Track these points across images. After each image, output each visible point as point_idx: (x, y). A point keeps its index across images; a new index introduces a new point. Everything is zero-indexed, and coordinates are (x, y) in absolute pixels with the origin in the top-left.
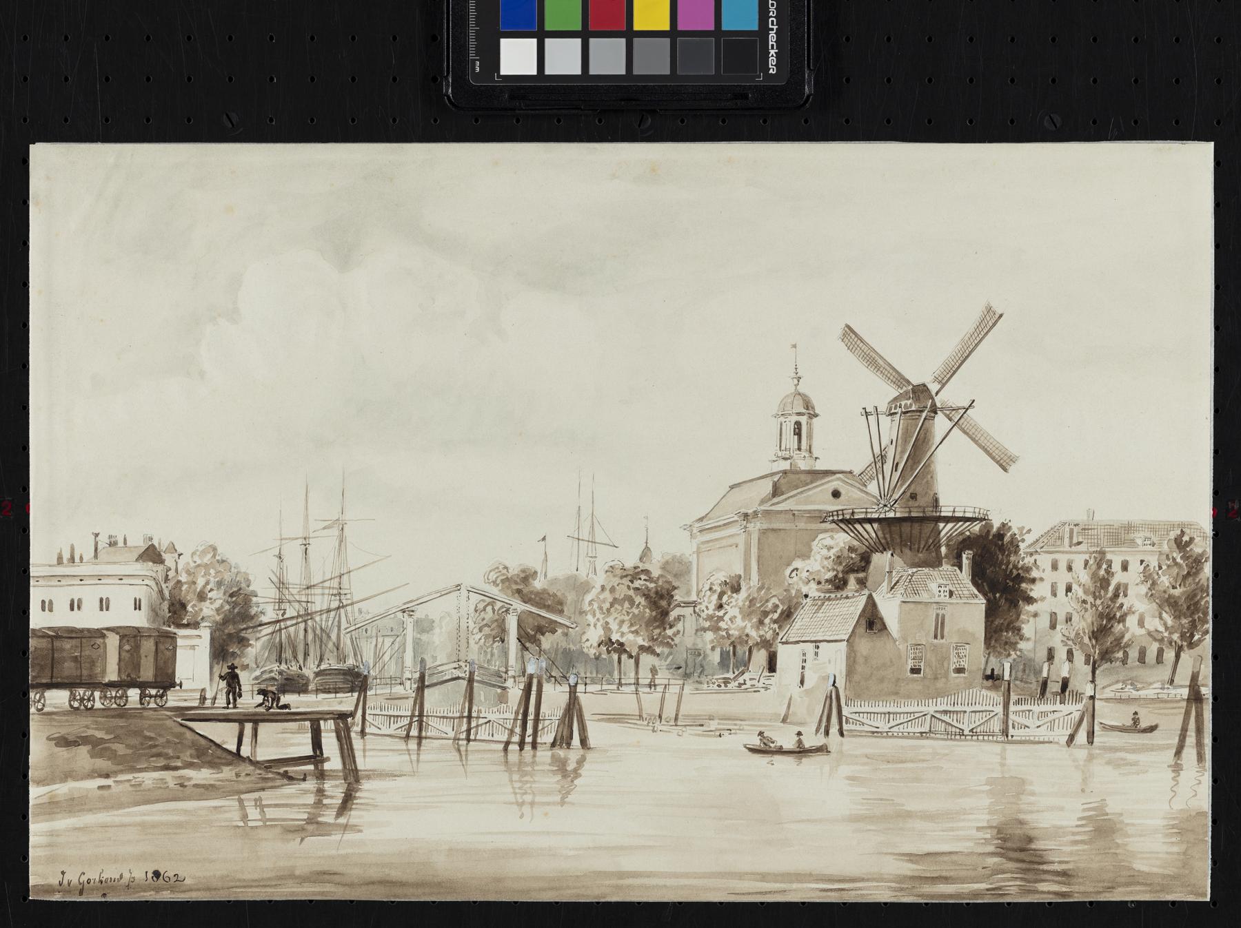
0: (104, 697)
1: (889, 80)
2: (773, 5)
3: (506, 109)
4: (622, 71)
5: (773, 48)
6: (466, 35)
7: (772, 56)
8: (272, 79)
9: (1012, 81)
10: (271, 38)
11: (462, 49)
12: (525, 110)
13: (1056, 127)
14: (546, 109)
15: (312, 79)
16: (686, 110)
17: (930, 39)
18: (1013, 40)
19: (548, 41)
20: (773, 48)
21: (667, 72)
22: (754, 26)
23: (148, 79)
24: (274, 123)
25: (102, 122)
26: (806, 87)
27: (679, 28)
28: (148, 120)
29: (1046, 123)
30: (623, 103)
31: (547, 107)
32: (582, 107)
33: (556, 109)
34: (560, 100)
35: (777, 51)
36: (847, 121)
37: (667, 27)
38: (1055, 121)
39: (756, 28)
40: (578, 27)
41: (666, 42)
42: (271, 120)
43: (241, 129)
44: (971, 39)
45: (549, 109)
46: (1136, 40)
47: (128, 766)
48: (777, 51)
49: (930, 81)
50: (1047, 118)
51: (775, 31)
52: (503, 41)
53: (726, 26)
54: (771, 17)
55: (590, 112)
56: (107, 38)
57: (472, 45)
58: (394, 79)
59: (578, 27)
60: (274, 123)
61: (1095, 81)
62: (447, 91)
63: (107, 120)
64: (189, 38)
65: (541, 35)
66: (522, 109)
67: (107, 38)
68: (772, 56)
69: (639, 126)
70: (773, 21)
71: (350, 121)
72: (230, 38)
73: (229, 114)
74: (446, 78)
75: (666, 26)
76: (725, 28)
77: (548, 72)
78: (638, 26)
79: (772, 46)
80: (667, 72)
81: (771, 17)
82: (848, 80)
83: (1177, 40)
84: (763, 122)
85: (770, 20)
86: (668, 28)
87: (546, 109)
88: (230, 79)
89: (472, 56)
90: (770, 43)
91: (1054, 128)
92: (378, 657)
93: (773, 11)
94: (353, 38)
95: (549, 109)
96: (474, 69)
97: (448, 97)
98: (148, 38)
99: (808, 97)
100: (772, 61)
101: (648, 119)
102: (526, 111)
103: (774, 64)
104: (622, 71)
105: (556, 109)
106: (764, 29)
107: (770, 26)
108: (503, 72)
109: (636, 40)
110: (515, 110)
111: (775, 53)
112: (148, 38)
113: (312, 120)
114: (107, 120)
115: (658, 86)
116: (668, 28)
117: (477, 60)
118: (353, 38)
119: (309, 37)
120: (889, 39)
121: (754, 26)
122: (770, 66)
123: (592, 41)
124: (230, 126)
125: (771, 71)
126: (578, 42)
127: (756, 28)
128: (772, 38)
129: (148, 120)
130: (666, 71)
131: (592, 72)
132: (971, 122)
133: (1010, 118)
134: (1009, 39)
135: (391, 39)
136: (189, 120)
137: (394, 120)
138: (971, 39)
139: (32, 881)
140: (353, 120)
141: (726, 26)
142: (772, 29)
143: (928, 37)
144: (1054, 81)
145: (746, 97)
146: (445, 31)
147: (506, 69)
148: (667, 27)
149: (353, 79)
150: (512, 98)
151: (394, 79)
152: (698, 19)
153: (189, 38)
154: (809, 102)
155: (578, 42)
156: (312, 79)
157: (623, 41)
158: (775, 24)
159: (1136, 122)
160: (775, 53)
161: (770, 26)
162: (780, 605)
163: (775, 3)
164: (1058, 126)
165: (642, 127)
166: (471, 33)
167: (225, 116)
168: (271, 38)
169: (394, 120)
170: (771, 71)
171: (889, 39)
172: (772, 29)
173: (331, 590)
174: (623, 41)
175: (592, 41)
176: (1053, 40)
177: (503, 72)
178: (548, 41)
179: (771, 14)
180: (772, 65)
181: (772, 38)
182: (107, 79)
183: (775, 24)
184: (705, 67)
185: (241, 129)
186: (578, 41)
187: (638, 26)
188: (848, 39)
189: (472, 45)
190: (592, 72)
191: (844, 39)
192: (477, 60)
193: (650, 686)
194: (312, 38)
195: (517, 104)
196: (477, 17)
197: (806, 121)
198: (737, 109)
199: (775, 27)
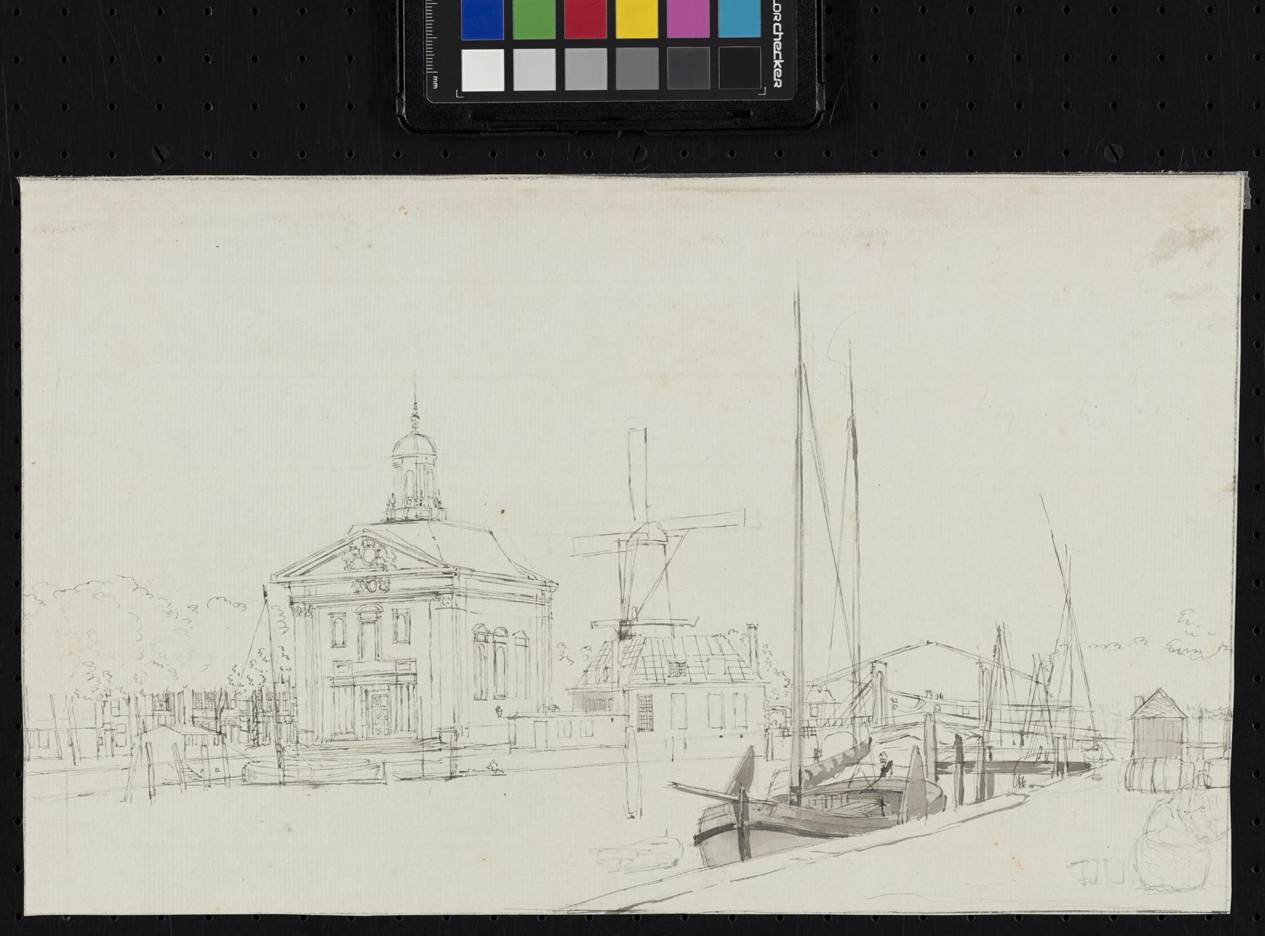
1: (923, 106)
2: (777, 8)
3: (469, 132)
4: (551, 86)
5: (777, 58)
6: (422, 46)
7: (777, 67)
8: (208, 107)
9: (1067, 106)
11: (416, 62)
12: (490, 132)
13: (1118, 159)
14: (516, 131)
15: (255, 107)
16: (677, 130)
17: (971, 58)
18: (1067, 58)
19: (517, 52)
20: (777, 58)
21: (656, 86)
22: (757, 34)
23: (65, 107)
24: (210, 158)
25: (11, 157)
26: (817, 103)
27: (670, 36)
28: (64, 155)
29: (1106, 154)
30: (604, 123)
31: (517, 129)
32: (557, 128)
33: (528, 131)
34: (532, 121)
35: (783, 61)
36: (875, 153)
37: (655, 35)
38: (1117, 152)
39: (758, 34)
41: (655, 51)
42: (207, 154)
43: (173, 165)
44: (1019, 58)
45: (519, 131)
46: (1210, 58)
48: (783, 61)
49: (971, 106)
50: (1107, 148)
51: (780, 38)
54: (776, 22)
55: (567, 133)
56: (17, 60)
57: (428, 57)
58: (350, 106)
60: (210, 158)
61: (1162, 105)
63: (17, 155)
64: (112, 59)
65: (509, 45)
66: (487, 131)
67: (17, 60)
68: (777, 67)
69: (634, 160)
70: (777, 27)
71: (299, 155)
72: (160, 59)
73: (159, 148)
74: (400, 95)
75: (654, 34)
76: (722, 35)
77: (518, 87)
78: (621, 34)
79: (777, 55)
80: (656, 86)
81: (776, 22)
82: (876, 106)
83: (1258, 58)
84: (778, 155)
85: (775, 25)
87: (516, 131)
88: (160, 107)
89: (429, 69)
90: (775, 52)
91: (1116, 161)
93: (777, 16)
95: (519, 131)
96: (431, 84)
98: (64, 60)
99: (819, 114)
100: (778, 73)
101: (644, 150)
102: (492, 134)
103: (779, 76)
104: (551, 86)
105: (528, 131)
106: (767, 36)
107: (775, 33)
108: (465, 89)
109: (619, 50)
110: (480, 132)
111: (781, 63)
112: (64, 60)
113: (255, 154)
114: (17, 155)
115: (645, 103)
117: (435, 75)
119: (251, 58)
120: (923, 58)
121: (757, 34)
122: (775, 79)
123: (568, 51)
124: (160, 161)
125: (776, 85)
127: (758, 34)
128: (777, 45)
129: (64, 155)
130: (655, 86)
132: (1019, 153)
133: (1065, 149)
135: (346, 59)
136: (112, 155)
137: (350, 154)
138: (1019, 58)
140: (302, 154)
142: (777, 36)
143: (969, 54)
144: (1115, 105)
145: (745, 114)
148: (655, 35)
149: (302, 107)
150: (476, 118)
151: (350, 106)
152: (690, 25)
153: (112, 59)
154: (820, 121)
156: (255, 107)
157: (604, 51)
158: (780, 30)
159: (1210, 153)
160: (781, 63)
161: (775, 33)
163: (780, 6)
164: (1120, 157)
165: (636, 161)
166: (428, 43)
167: (153, 150)
168: (207, 59)
169: (350, 154)
171: (923, 58)
172: (777, 36)
173: (282, 719)
174: (604, 51)
175: (568, 51)
176: (1114, 58)
177: (465, 89)
178: (517, 52)
179: (776, 18)
180: (777, 78)
181: (777, 45)
182: (17, 107)
183: (780, 30)
185: (173, 165)
186: (552, 52)
187: (621, 34)
188: (875, 58)
189: (428, 57)
191: (871, 57)
192: (435, 75)
194: (255, 59)
195: (482, 125)
196: (434, 25)
197: (828, 153)
198: (738, 130)
199: (780, 34)
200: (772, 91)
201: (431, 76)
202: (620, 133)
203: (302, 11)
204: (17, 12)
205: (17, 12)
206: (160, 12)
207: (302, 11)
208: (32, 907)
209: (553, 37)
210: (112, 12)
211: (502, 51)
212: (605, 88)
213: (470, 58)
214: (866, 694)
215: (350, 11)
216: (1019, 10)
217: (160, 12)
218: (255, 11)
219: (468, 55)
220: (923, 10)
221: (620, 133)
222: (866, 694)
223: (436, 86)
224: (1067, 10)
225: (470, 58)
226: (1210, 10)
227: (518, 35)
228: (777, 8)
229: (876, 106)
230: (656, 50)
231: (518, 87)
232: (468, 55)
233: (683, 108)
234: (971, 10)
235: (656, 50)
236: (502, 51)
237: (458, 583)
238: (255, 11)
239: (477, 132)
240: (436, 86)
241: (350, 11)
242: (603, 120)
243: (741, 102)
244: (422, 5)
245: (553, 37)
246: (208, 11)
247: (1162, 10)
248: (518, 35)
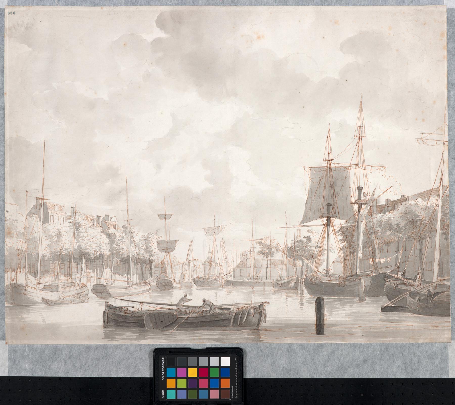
0: (437, 344)
4: (175, 398)
19: (218, 365)
22: (168, 369)
37: (189, 369)
41: (189, 365)
52: (229, 365)
65: (220, 367)
77: (218, 358)
78: (186, 380)
89: (237, 362)
92: (387, 217)
93: (163, 373)
100: (163, 361)
104: (175, 398)
108: (229, 358)
121: (168, 369)
126: (200, 391)
128: (163, 366)
130: (189, 358)
131: (207, 358)
139: (149, 377)
147: (228, 358)
148: (189, 369)
155: (200, 391)
162: (107, 285)
177: (229, 358)
178: (178, 369)
181: (163, 366)
184: (179, 359)
196: (235, 364)
200: (164, 357)
201: (236, 360)
211: (221, 387)
213: (228, 386)
214: (215, 256)
222: (215, 256)
223: (235, 358)
225: (228, 386)
227: (218, 369)
236: (221, 387)
237: (112, 315)
240: (235, 358)
248: (218, 369)
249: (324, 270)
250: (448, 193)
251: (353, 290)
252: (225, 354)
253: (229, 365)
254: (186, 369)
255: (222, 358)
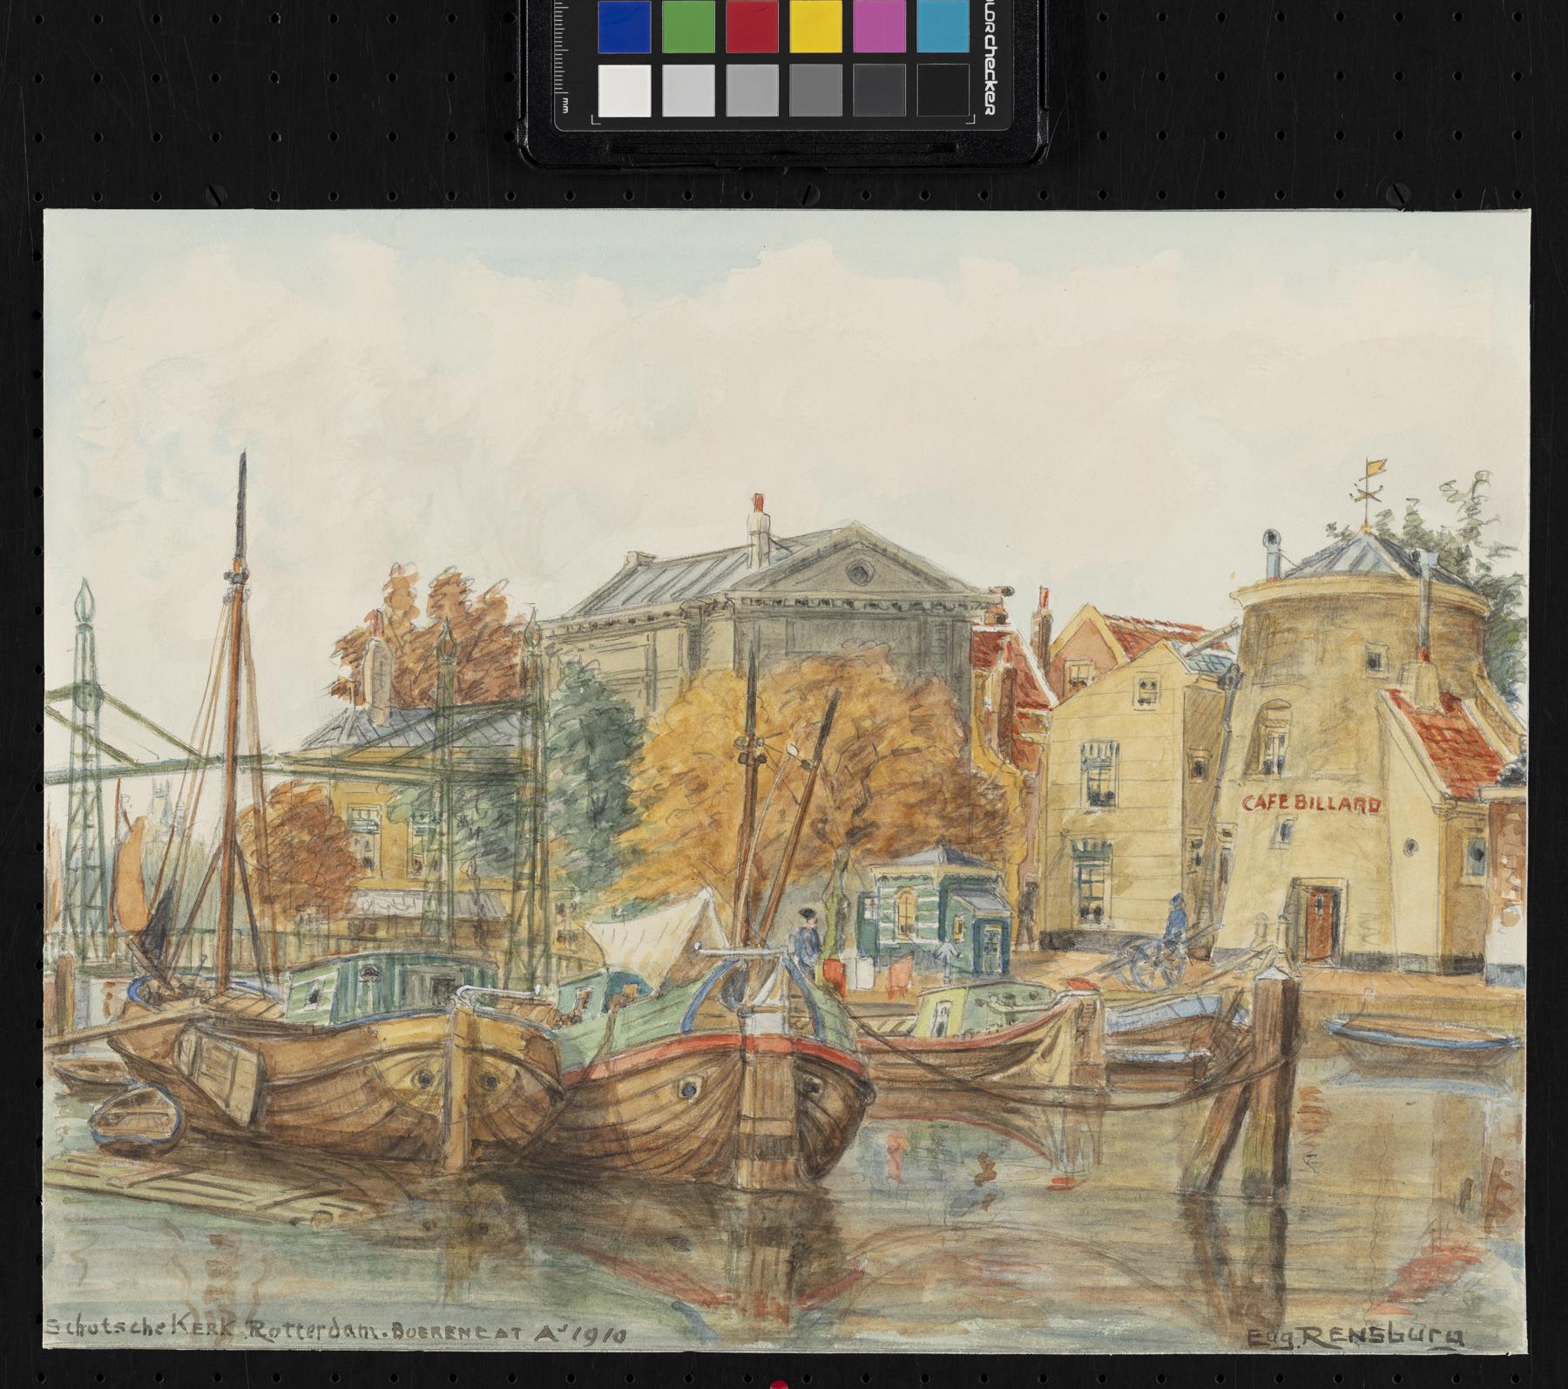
1: (1162, 136)
2: (990, 16)
3: (606, 167)
4: (709, 111)
5: (990, 79)
6: (549, 61)
8: (275, 137)
9: (1340, 136)
10: (275, 78)
15: (334, 137)
17: (1221, 76)
18: (1340, 76)
19: (903, 49)
20: (990, 79)
21: (839, 113)
22: (964, 47)
23: (97, 138)
39: (965, 49)
40: (710, 47)
41: (838, 68)
44: (1281, 76)
46: (1518, 76)
47: (75, 847)
49: (1221, 136)
50: (1390, 189)
52: (603, 69)
53: (923, 47)
56: (38, 79)
58: (452, 137)
59: (710, 47)
61: (1459, 135)
62: (522, 140)
64: (156, 78)
65: (657, 60)
66: (629, 167)
67: (38, 79)
70: (990, 40)
72: (215, 78)
74: (521, 121)
75: (836, 47)
77: (731, 112)
78: (795, 48)
79: (990, 74)
80: (839, 113)
82: (1103, 136)
85: (987, 37)
86: (839, 50)
88: (216, 137)
89: (558, 89)
90: (987, 71)
93: (990, 26)
94: (392, 78)
96: (561, 108)
97: (524, 150)
98: (97, 79)
99: (1042, 148)
100: (990, 96)
104: (709, 111)
107: (987, 47)
108: (602, 114)
109: (793, 67)
112: (97, 79)
116: (839, 50)
117: (565, 96)
118: (392, 78)
120: (1162, 77)
121: (964, 47)
123: (731, 68)
125: (988, 112)
126: (709, 70)
127: (965, 49)
128: (990, 63)
130: (838, 112)
134: (1335, 75)
141: (923, 47)
142: (990, 52)
144: (1399, 136)
145: (951, 148)
146: (519, 53)
149: (393, 137)
150: (615, 150)
151: (452, 137)
152: (881, 36)
153: (156, 78)
155: (709, 70)
156: (334, 137)
157: (775, 68)
161: (987, 47)
167: (208, 190)
168: (275, 78)
170: (988, 112)
171: (1162, 77)
172: (990, 52)
174: (775, 68)
175: (731, 68)
176: (1399, 76)
177: (602, 114)
178: (903, 49)
179: (988, 29)
181: (990, 63)
182: (39, 138)
187: (795, 48)
188: (1103, 77)
190: (730, 113)
193: (710, 608)
194: (333, 78)
199: (994, 49)
200: (983, 119)
202: (786, 170)
203: (393, 18)
204: (38, 20)
205: (38, 20)
206: (216, 19)
207: (393, 18)
208: (53, 218)
209: (712, 50)
210: (156, 19)
212: (648, 114)
213: (608, 75)
215: (452, 18)
216: (1281, 17)
217: (216, 19)
218: (334, 19)
219: (606, 72)
220: (1162, 17)
221: (786, 170)
224: (1340, 17)
225: (608, 75)
226: (1518, 17)
228: (990, 16)
229: (1103, 136)
230: (839, 67)
231: (731, 112)
232: (606, 72)
233: (872, 139)
234: (1221, 17)
235: (839, 67)
238: (334, 19)
239: (618, 168)
241: (452, 18)
242: (773, 154)
243: (944, 133)
244: (550, 10)
245: (712, 50)
246: (275, 19)
247: (1459, 17)
248: (667, 49)
249: (534, 612)
250: (69, 703)
251: (950, 860)
252: (632, 135)
253: (603, 69)
254: (857, 49)
255: (641, 108)
